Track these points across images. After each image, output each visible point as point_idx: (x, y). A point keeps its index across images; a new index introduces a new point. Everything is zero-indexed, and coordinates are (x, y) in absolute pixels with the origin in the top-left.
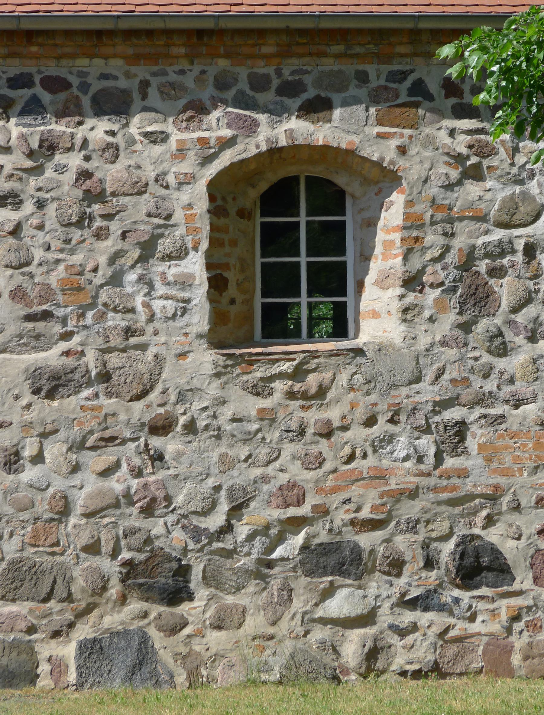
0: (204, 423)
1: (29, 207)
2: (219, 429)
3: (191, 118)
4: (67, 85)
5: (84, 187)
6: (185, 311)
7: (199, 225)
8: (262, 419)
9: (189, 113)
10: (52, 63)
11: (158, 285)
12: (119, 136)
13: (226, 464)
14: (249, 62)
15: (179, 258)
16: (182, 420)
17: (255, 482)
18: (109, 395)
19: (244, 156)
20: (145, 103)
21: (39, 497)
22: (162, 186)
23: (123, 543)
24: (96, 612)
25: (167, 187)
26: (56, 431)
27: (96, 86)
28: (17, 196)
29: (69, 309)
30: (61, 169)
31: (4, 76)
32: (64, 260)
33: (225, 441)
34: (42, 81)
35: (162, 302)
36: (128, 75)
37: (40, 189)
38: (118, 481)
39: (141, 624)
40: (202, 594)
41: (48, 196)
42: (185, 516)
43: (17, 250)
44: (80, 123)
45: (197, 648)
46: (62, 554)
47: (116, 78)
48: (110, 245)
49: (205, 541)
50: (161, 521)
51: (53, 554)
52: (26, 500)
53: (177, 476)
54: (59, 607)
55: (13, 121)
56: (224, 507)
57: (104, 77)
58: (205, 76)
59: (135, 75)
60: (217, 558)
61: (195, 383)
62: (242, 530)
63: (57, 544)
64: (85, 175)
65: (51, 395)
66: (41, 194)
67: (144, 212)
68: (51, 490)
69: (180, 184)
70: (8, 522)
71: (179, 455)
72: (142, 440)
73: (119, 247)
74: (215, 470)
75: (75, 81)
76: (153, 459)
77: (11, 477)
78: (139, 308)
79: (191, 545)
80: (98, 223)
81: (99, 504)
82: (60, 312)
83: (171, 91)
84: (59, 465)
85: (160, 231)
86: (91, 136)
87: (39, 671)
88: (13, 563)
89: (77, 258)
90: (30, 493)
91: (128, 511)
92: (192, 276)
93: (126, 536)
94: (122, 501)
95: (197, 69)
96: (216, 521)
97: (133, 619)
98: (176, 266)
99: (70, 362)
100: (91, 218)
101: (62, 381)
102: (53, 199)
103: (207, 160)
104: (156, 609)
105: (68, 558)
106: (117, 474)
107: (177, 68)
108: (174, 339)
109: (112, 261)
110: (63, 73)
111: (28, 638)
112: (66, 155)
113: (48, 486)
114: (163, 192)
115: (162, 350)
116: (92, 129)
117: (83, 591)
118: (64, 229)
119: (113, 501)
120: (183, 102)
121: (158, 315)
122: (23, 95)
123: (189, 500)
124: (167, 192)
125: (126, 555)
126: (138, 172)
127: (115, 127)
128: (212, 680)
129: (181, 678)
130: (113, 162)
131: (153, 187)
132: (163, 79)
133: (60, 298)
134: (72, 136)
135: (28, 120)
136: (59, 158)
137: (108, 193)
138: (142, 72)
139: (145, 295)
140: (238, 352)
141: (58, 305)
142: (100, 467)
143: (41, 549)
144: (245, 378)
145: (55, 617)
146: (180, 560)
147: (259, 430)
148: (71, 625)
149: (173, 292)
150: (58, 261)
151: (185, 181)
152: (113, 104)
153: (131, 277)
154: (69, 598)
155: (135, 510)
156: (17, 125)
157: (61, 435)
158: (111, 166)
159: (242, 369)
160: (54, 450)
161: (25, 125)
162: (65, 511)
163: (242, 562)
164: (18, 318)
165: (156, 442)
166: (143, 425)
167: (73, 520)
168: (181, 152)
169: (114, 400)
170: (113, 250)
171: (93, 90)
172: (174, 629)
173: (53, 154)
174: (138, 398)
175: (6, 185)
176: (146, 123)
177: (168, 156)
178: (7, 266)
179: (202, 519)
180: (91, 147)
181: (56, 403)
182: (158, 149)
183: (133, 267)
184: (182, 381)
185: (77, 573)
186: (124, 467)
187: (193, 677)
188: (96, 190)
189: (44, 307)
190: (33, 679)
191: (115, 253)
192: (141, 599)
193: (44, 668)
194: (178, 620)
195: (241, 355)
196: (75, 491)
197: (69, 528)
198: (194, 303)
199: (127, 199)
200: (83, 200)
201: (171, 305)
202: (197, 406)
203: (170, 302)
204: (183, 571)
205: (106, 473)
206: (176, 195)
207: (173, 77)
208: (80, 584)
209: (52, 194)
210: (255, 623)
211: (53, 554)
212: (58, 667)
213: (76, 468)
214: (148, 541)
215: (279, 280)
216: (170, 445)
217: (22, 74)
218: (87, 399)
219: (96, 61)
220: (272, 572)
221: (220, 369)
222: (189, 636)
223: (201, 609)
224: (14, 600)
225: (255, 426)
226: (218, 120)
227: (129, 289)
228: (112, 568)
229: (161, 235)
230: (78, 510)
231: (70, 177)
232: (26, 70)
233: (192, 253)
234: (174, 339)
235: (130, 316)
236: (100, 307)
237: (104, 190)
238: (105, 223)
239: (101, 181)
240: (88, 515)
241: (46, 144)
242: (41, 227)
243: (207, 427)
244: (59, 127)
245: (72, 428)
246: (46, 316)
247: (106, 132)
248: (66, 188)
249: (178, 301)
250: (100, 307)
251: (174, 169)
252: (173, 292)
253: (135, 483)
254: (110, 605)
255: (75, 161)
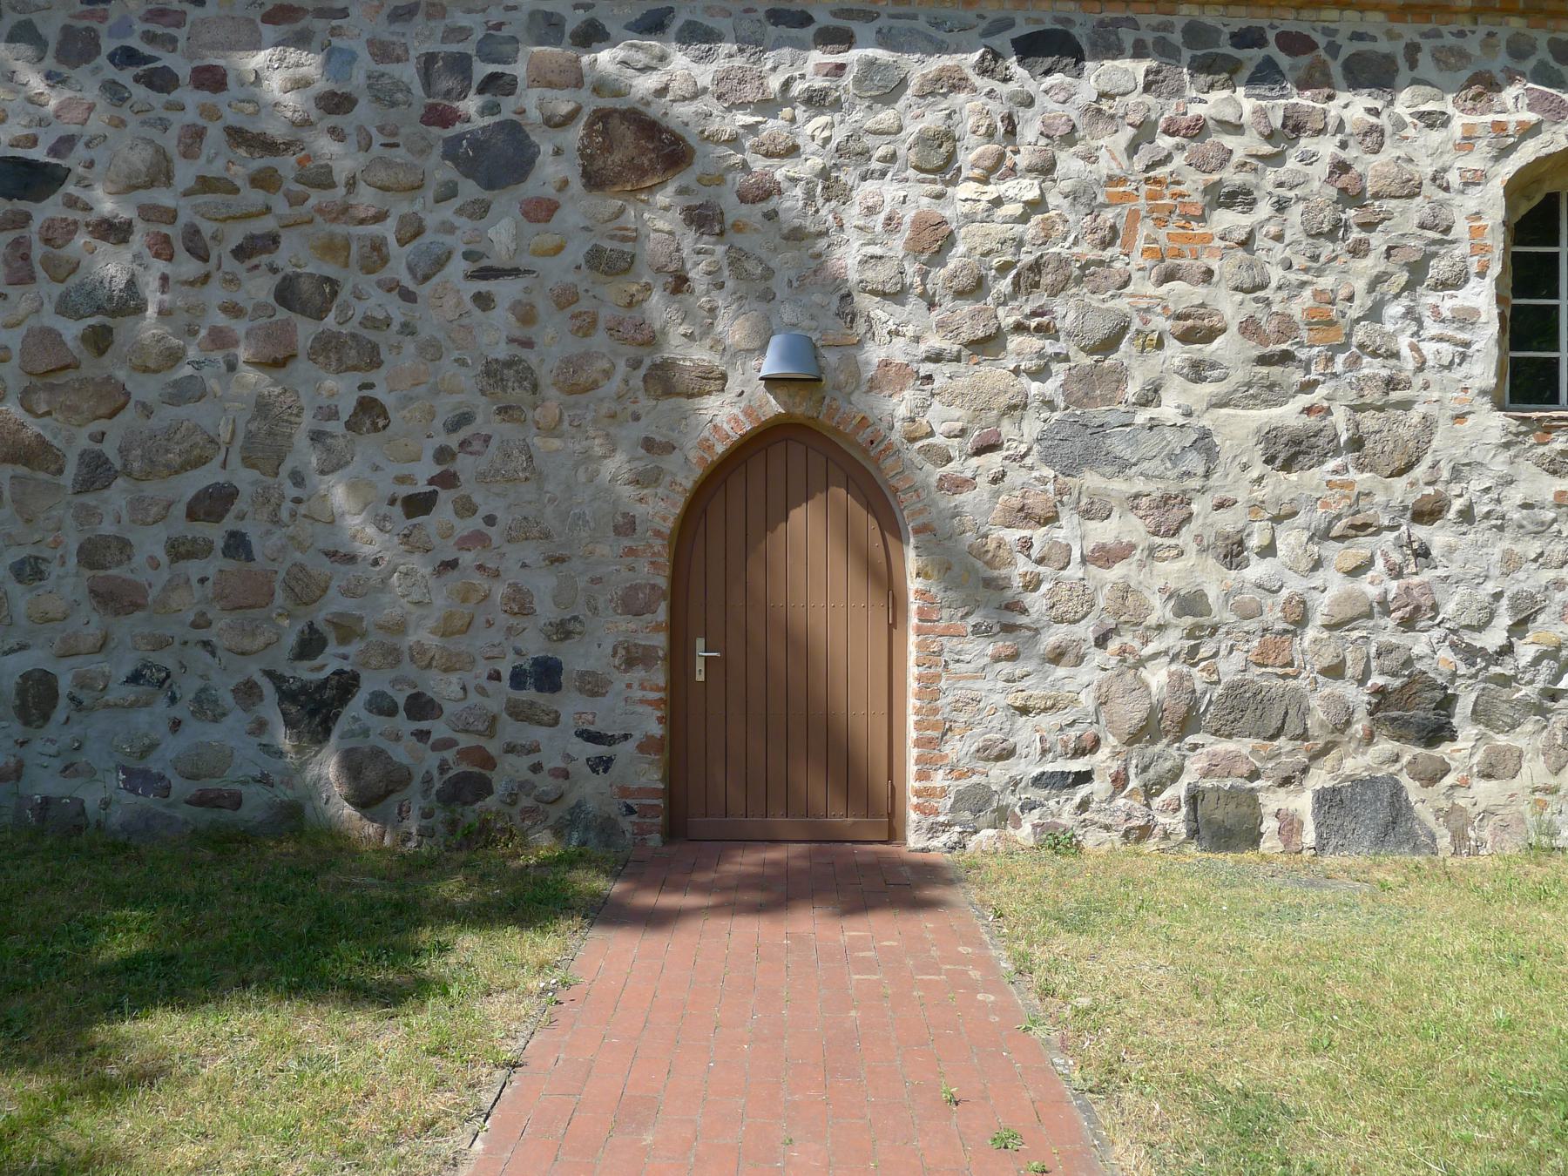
0: (1486, 509)
1: (1264, 209)
2: (1503, 517)
3: (1480, 95)
4: (1311, 46)
5: (1339, 185)
6: (1464, 357)
7: (1489, 242)
8: (1559, 506)
9: (1476, 89)
10: (1291, 14)
11: (1428, 322)
12: (1384, 116)
13: (1511, 563)
14: (1551, 24)
15: (1456, 287)
16: (1457, 505)
17: (1547, 588)
18: (1361, 468)
19: (1552, 149)
20: (1415, 74)
21: (1270, 602)
22: (1440, 186)
23: (1374, 664)
24: (1334, 753)
25: (1447, 189)
26: (1295, 514)
27: (1349, 48)
28: (1249, 193)
29: (1315, 350)
30: (1308, 159)
31: (1226, 30)
32: (1312, 283)
33: (1508, 534)
34: (1278, 37)
35: (1434, 346)
36: (1391, 36)
37: (1281, 185)
38: (1371, 583)
39: (1392, 770)
40: (1467, 733)
41: (1291, 194)
42: (1453, 631)
43: (1250, 267)
44: (1330, 98)
45: (1461, 802)
46: (1296, 677)
47: (1374, 39)
48: (1371, 264)
49: (1480, 663)
50: (1424, 637)
51: (1285, 677)
52: (1254, 605)
53: (1447, 577)
54: (1289, 746)
55: (1241, 91)
56: (1504, 620)
57: (1357, 36)
58: (1493, 41)
59: (1400, 36)
60: (1492, 686)
61: (1476, 455)
62: (1526, 652)
63: (1290, 664)
64: (1341, 167)
65: (1287, 466)
66: (1283, 192)
67: (1416, 222)
68: (1285, 593)
69: (1466, 184)
70: (1227, 633)
71: (1451, 550)
72: (1404, 528)
73: (1382, 269)
74: (1495, 572)
75: (1321, 41)
76: (1416, 554)
77: (1233, 573)
78: (1405, 352)
79: (1463, 669)
80: (1356, 234)
81: (1349, 612)
82: (1302, 354)
83: (1450, 59)
84: (1296, 560)
85: (1433, 248)
86: (1346, 114)
87: (1263, 829)
88: (1232, 687)
89: (1326, 282)
90: (1259, 595)
91: (1382, 622)
92: (1476, 312)
93: (1379, 655)
94: (1377, 609)
95: (1482, 30)
96: (1493, 639)
97: (1383, 763)
98: (1452, 297)
99: (1312, 421)
100: (1347, 228)
101: (1303, 448)
102: (1298, 199)
103: (1504, 152)
104: (1410, 752)
105: (1302, 683)
106: (1370, 574)
107: (1455, 28)
108: (1450, 395)
109: (1372, 287)
110: (1304, 28)
111: (1249, 785)
112: (1315, 140)
113: (1281, 587)
114: (1442, 195)
115: (1434, 410)
116: (1346, 106)
117: (1322, 725)
118: (1310, 241)
119: (1366, 609)
120: (1465, 74)
121: (1430, 363)
122: (1252, 57)
123: (1462, 609)
124: (1447, 195)
125: (1377, 680)
126: (1410, 167)
127: (1379, 104)
128: (1481, 843)
129: (1444, 841)
130: (1376, 152)
131: (1428, 188)
132: (1438, 42)
133: (1305, 335)
134: (1325, 112)
135: (1262, 90)
136: (1305, 143)
137: (1368, 195)
138: (1409, 31)
139: (1412, 336)
140: (1535, 415)
141: (1301, 345)
142: (1350, 564)
143: (1269, 670)
144: (1541, 450)
145: (1283, 759)
146: (1446, 688)
147: (1555, 520)
148: (1305, 770)
149: (1449, 332)
150: (1303, 284)
151: (1474, 181)
152: (1374, 74)
153: (1395, 310)
154: (1304, 736)
155: (1390, 622)
156: (1247, 96)
157: (1301, 519)
158: (1373, 157)
159: (1537, 438)
160: (1290, 539)
161: (1259, 97)
162: (1302, 622)
163: (1525, 692)
164: (1248, 360)
165: (1421, 532)
166: (1406, 508)
167: (1311, 633)
168: (1468, 141)
169: (1366, 475)
170: (1375, 272)
171: (1344, 54)
172: (1432, 776)
173: (1298, 137)
174: (1400, 473)
175: (1235, 177)
176: (1419, 100)
177: (1450, 146)
178: (1236, 289)
179: (1476, 635)
180: (1348, 130)
181: (1293, 477)
182: (1436, 136)
183: (1397, 296)
184: (1459, 452)
185: (1314, 702)
186: (1380, 563)
187: (1459, 838)
188: (1353, 191)
189: (1284, 346)
190: (1254, 839)
191: (1377, 276)
192: (1391, 738)
193: (1269, 825)
194: (1438, 765)
195: (1539, 420)
196: (1316, 594)
197: (1306, 644)
198: (1475, 347)
199: (1394, 203)
200: (1337, 202)
201: (1446, 347)
202: (1476, 485)
203: (1445, 345)
204: (1447, 703)
205: (1356, 572)
206: (1458, 199)
207: (1450, 40)
208: (1318, 715)
209: (1297, 191)
210: (1534, 770)
211: (1285, 677)
212: (1289, 825)
213: (1317, 565)
214: (1408, 662)
216: (1437, 537)
217: (1249, 28)
218: (1335, 472)
219: (1348, 14)
220: (1557, 706)
221: (1510, 437)
222: (1452, 787)
223: (1467, 752)
224: (1230, 736)
225: (1551, 515)
226: (1517, 98)
227: (1389, 327)
228: (1359, 697)
229: (1435, 255)
230: (1318, 619)
231: (1321, 169)
232: (1255, 23)
233: (1474, 281)
234: (1450, 395)
235: (1393, 362)
236: (1354, 349)
237: (1364, 189)
238: (1363, 235)
239: (1361, 177)
240: (1329, 627)
241: (1290, 123)
242: (1279, 238)
243: (1488, 515)
244: (1304, 100)
245: (1315, 510)
246: (1286, 358)
247: (1369, 111)
248: (1316, 185)
249: (1456, 345)
250: (1354, 349)
251: (1458, 164)
252: (1449, 332)
253: (1394, 586)
254: (1353, 745)
255: (1327, 148)
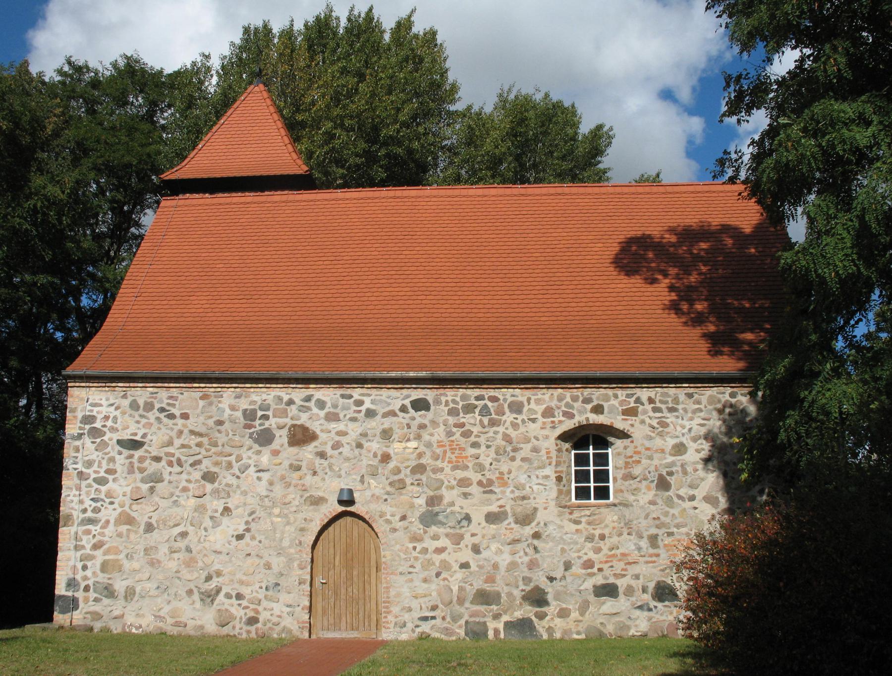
1: (483, 448)
57: (513, 396)
75: (501, 397)
110: (496, 394)
132: (536, 397)
171: (508, 402)
207: (540, 396)
215: (582, 476)
